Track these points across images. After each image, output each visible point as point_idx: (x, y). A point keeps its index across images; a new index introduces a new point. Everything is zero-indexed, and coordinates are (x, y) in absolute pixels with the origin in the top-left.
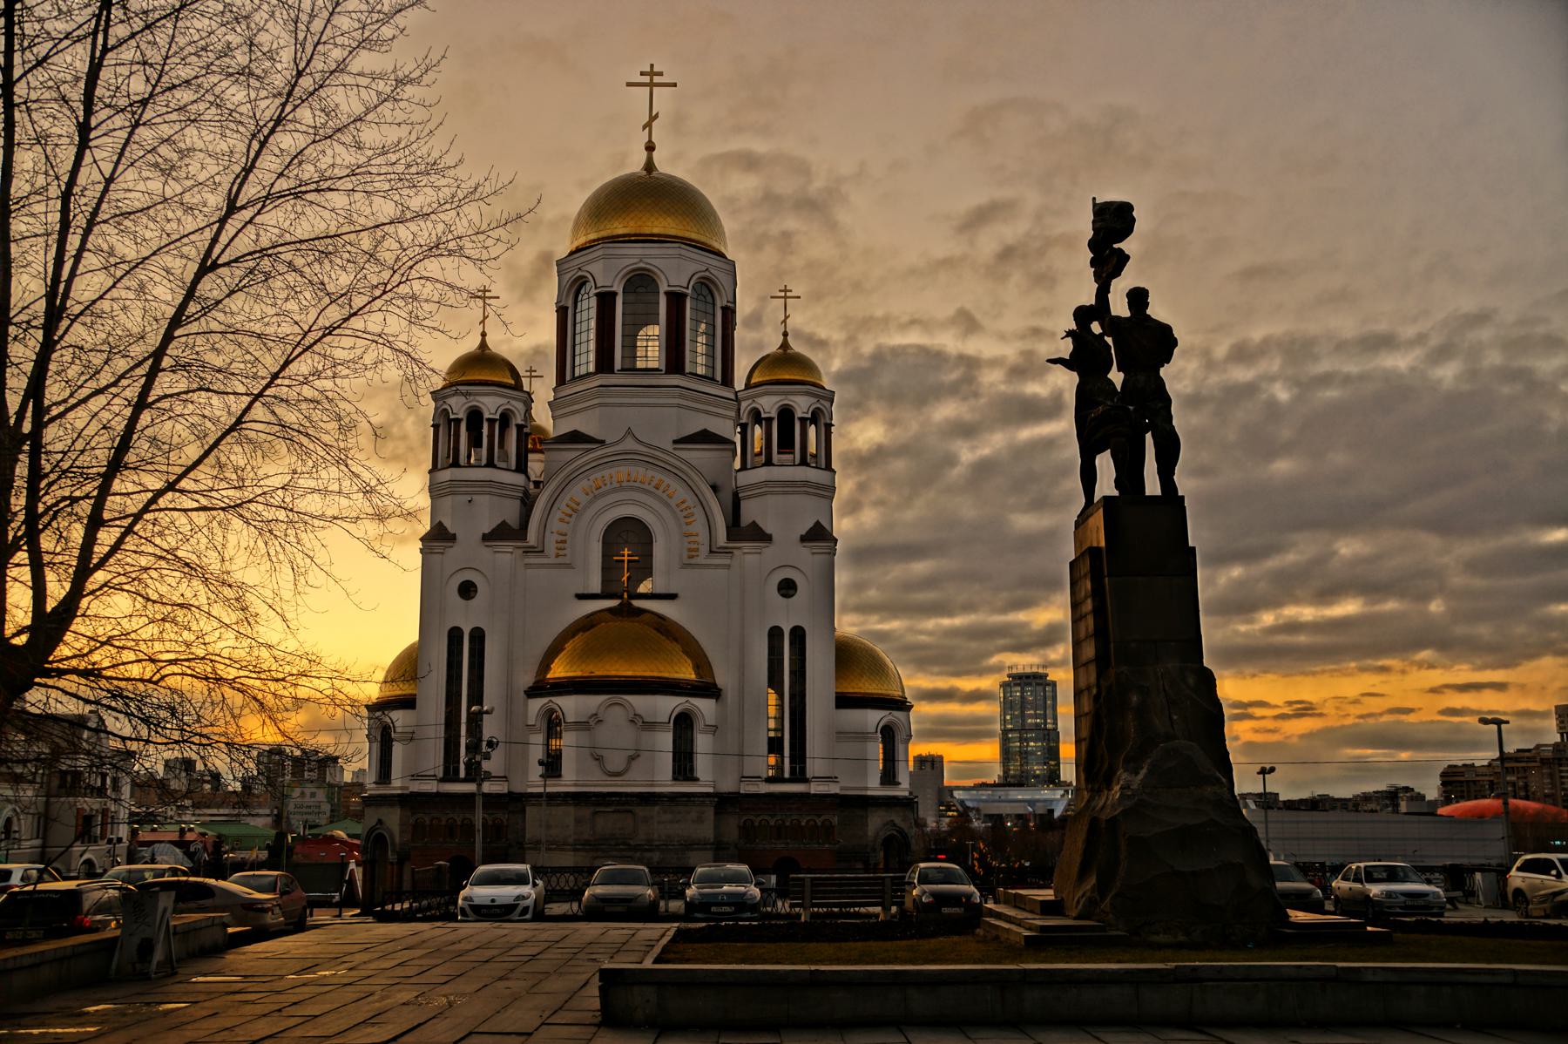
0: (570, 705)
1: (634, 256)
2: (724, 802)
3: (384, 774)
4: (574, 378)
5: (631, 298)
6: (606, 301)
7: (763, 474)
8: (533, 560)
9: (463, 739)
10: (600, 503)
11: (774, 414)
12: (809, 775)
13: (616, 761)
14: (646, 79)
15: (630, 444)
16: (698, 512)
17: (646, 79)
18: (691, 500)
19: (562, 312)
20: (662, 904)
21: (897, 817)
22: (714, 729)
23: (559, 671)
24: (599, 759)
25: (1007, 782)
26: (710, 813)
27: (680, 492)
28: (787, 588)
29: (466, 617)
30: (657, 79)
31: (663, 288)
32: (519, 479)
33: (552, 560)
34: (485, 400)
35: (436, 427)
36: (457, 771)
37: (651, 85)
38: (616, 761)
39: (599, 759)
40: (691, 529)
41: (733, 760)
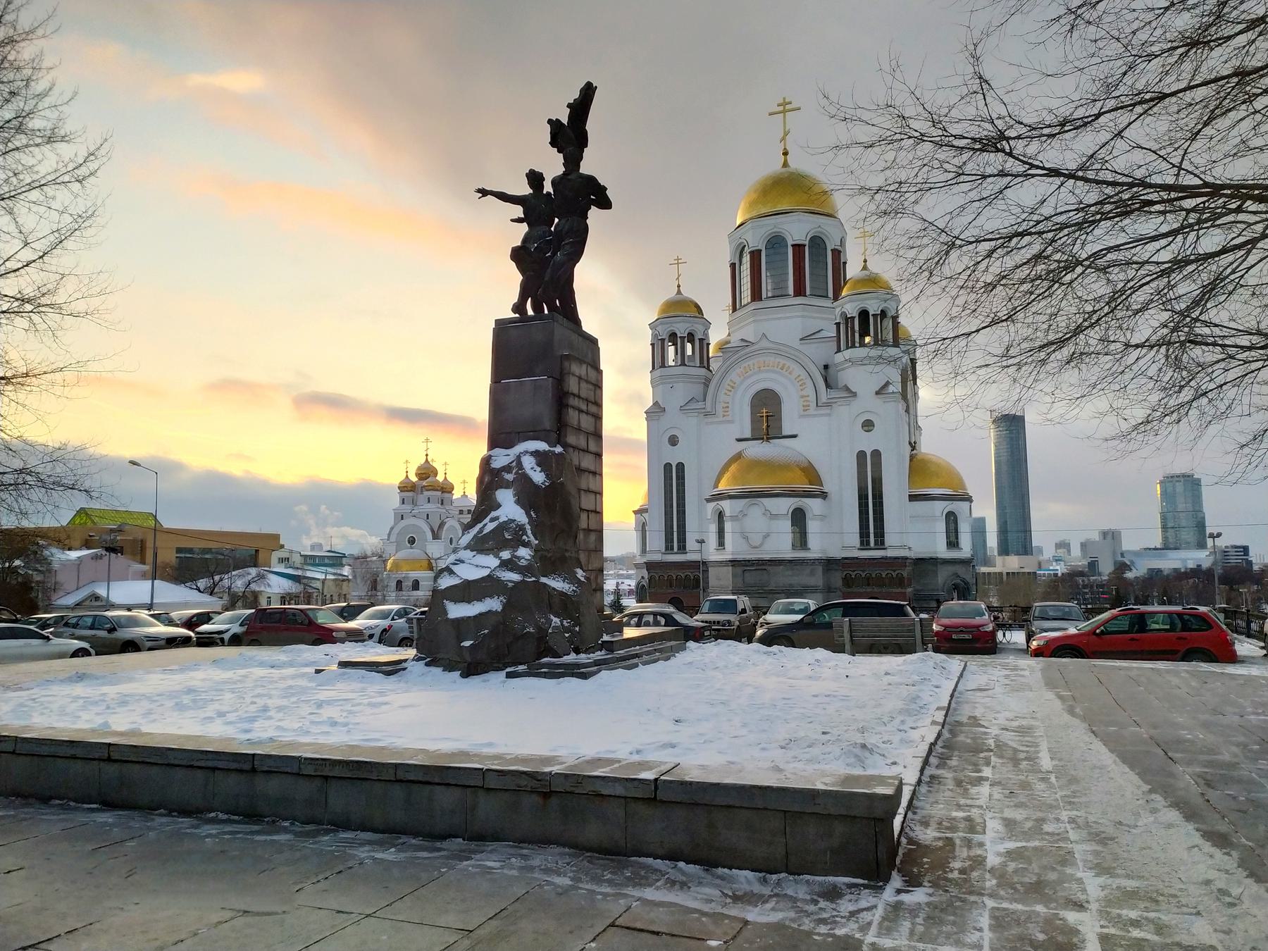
0: (726, 505)
1: (771, 226)
2: (829, 564)
3: (644, 551)
4: (742, 307)
5: (772, 251)
6: (755, 255)
7: (848, 354)
8: (710, 419)
9: (675, 531)
10: (749, 381)
11: (855, 314)
12: (887, 544)
13: (756, 540)
14: (781, 108)
15: (764, 344)
16: (809, 382)
17: (781, 108)
18: (803, 374)
19: (733, 266)
20: (1000, 635)
21: (960, 570)
22: (823, 517)
23: (723, 486)
24: (746, 538)
25: (1166, 547)
26: (820, 570)
27: (798, 371)
28: (868, 425)
29: (868, 443)
30: (788, 107)
31: (790, 242)
32: (703, 371)
33: (721, 419)
34: (678, 325)
35: (653, 345)
36: (868, 543)
37: (784, 112)
38: (756, 540)
39: (746, 538)
40: (804, 393)
41: (835, 534)
